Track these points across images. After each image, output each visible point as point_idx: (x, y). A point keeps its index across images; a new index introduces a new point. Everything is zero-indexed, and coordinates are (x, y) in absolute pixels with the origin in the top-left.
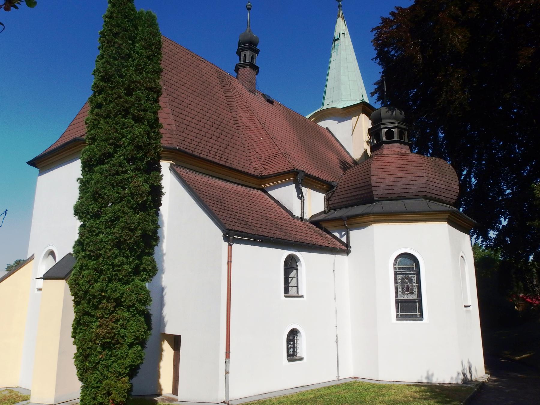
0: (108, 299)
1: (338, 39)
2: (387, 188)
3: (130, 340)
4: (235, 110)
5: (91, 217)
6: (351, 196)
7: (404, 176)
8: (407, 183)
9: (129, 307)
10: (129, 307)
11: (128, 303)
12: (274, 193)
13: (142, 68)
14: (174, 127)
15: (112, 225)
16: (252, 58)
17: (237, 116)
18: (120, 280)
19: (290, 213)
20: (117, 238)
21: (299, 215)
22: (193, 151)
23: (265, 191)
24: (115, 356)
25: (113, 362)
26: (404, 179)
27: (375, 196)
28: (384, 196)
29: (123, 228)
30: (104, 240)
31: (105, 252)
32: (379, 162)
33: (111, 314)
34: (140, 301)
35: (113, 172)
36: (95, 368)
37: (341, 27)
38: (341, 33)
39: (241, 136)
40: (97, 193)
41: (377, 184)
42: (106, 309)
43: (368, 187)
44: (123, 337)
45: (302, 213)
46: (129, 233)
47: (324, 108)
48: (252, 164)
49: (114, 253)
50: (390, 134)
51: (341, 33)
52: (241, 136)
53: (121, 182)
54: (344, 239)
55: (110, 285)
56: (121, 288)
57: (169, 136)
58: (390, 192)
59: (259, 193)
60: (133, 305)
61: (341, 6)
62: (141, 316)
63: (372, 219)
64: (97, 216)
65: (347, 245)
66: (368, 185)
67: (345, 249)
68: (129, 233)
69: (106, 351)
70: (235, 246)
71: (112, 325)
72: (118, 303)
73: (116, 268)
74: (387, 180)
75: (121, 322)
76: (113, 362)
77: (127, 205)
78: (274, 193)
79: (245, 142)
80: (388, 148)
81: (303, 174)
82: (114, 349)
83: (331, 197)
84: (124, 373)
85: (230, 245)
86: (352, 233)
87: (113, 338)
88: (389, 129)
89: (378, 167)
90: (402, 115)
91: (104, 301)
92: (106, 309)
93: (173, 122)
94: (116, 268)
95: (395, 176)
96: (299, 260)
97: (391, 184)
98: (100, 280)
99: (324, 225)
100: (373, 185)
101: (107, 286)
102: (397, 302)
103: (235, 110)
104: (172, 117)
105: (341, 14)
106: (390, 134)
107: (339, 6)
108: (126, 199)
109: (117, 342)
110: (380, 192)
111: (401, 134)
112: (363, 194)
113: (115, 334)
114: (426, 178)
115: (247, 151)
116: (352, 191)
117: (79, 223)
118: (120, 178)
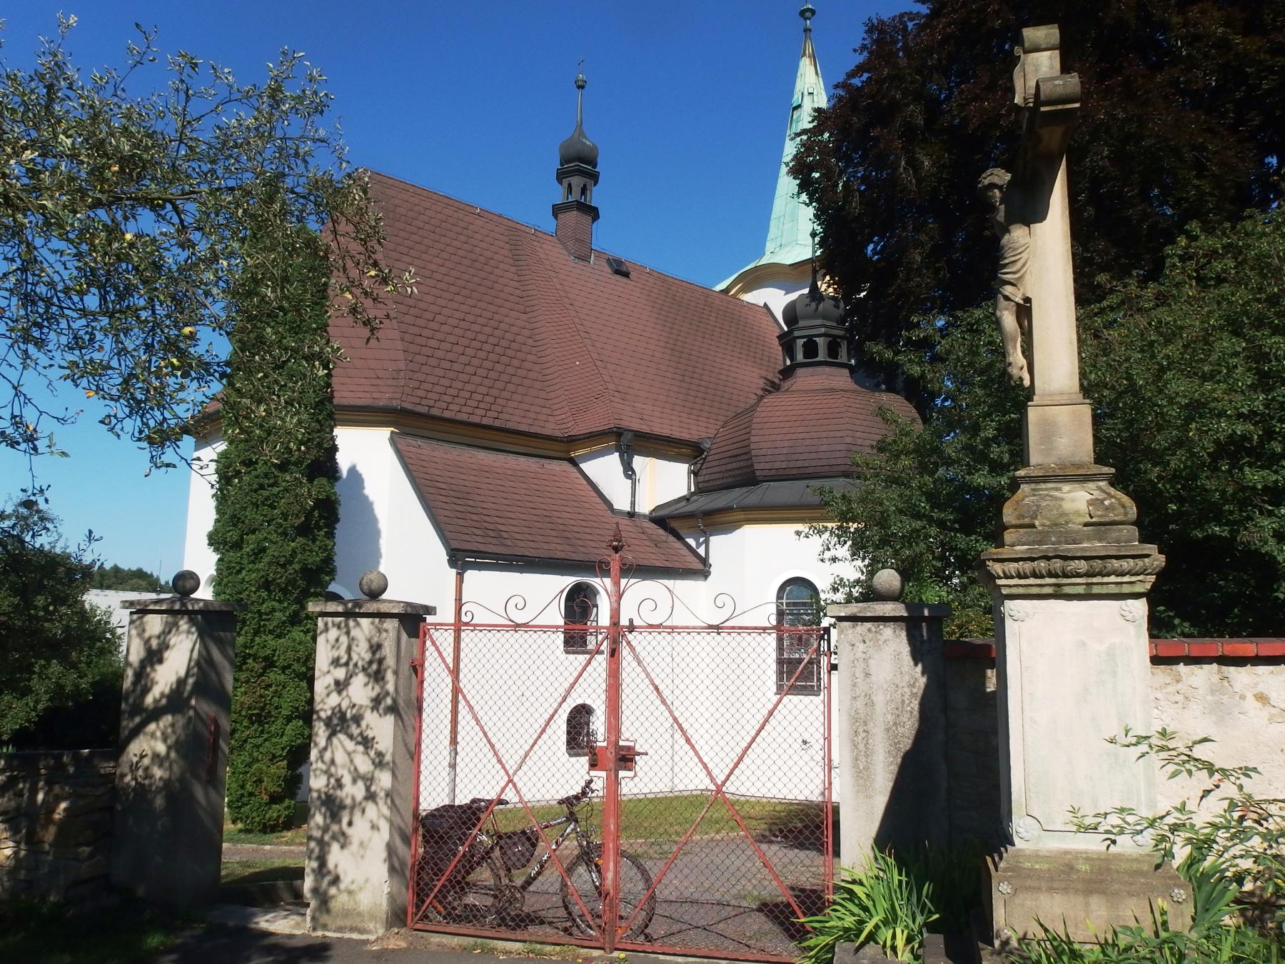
0: (255, 658)
1: (799, 106)
2: (779, 458)
3: (285, 712)
4: (534, 308)
5: (231, 548)
6: (727, 471)
7: (808, 436)
8: (814, 449)
9: (284, 669)
10: (284, 669)
11: (281, 663)
12: (589, 467)
13: (298, 326)
14: (402, 366)
15: (256, 559)
16: (584, 190)
17: (538, 319)
18: (271, 632)
19: (609, 504)
20: (263, 577)
21: (627, 508)
22: (430, 407)
23: (574, 462)
24: (268, 733)
25: (266, 740)
26: (808, 442)
27: (758, 473)
28: (773, 472)
29: (270, 563)
30: (247, 579)
31: (248, 595)
32: (769, 409)
33: (259, 677)
34: (298, 660)
35: (255, 486)
36: (241, 747)
37: (807, 80)
38: (806, 93)
39: (542, 360)
40: (234, 516)
41: (762, 452)
42: (252, 671)
43: (746, 457)
44: (277, 708)
45: (633, 504)
46: (279, 570)
47: (764, 261)
48: (554, 413)
49: (260, 596)
50: (810, 349)
51: (806, 93)
52: (542, 360)
53: (267, 498)
54: (701, 551)
55: (257, 639)
56: (273, 643)
57: (390, 382)
58: (784, 465)
59: (566, 466)
60: (289, 666)
61: (810, 30)
62: (301, 680)
63: (742, 517)
64: (238, 545)
65: (705, 561)
66: (745, 453)
67: (701, 570)
68: (279, 570)
69: (256, 726)
70: (470, 575)
71: (260, 691)
72: (269, 663)
73: (264, 617)
74: (778, 444)
75: (274, 688)
76: (266, 740)
77: (276, 531)
78: (589, 467)
79: (547, 371)
80: (806, 379)
81: (630, 435)
82: (267, 723)
83: (700, 469)
84: (280, 756)
85: (460, 576)
86: (715, 540)
87: (262, 709)
88: (810, 338)
89: (765, 420)
90: (838, 308)
91: (250, 661)
92: (252, 671)
93: (401, 355)
94: (264, 617)
95: (794, 437)
96: (598, 592)
97: (785, 451)
98: (243, 632)
99: (674, 524)
100: (754, 453)
101: (252, 641)
102: (780, 662)
103: (534, 308)
104: (399, 345)
105: (809, 50)
106: (810, 349)
107: (807, 30)
108: (898, 144)
109: (269, 715)
110: (768, 466)
111: (833, 350)
112: (741, 468)
113: (265, 705)
114: (848, 440)
115: (548, 389)
116: (727, 460)
117: (216, 557)
118: (266, 493)
